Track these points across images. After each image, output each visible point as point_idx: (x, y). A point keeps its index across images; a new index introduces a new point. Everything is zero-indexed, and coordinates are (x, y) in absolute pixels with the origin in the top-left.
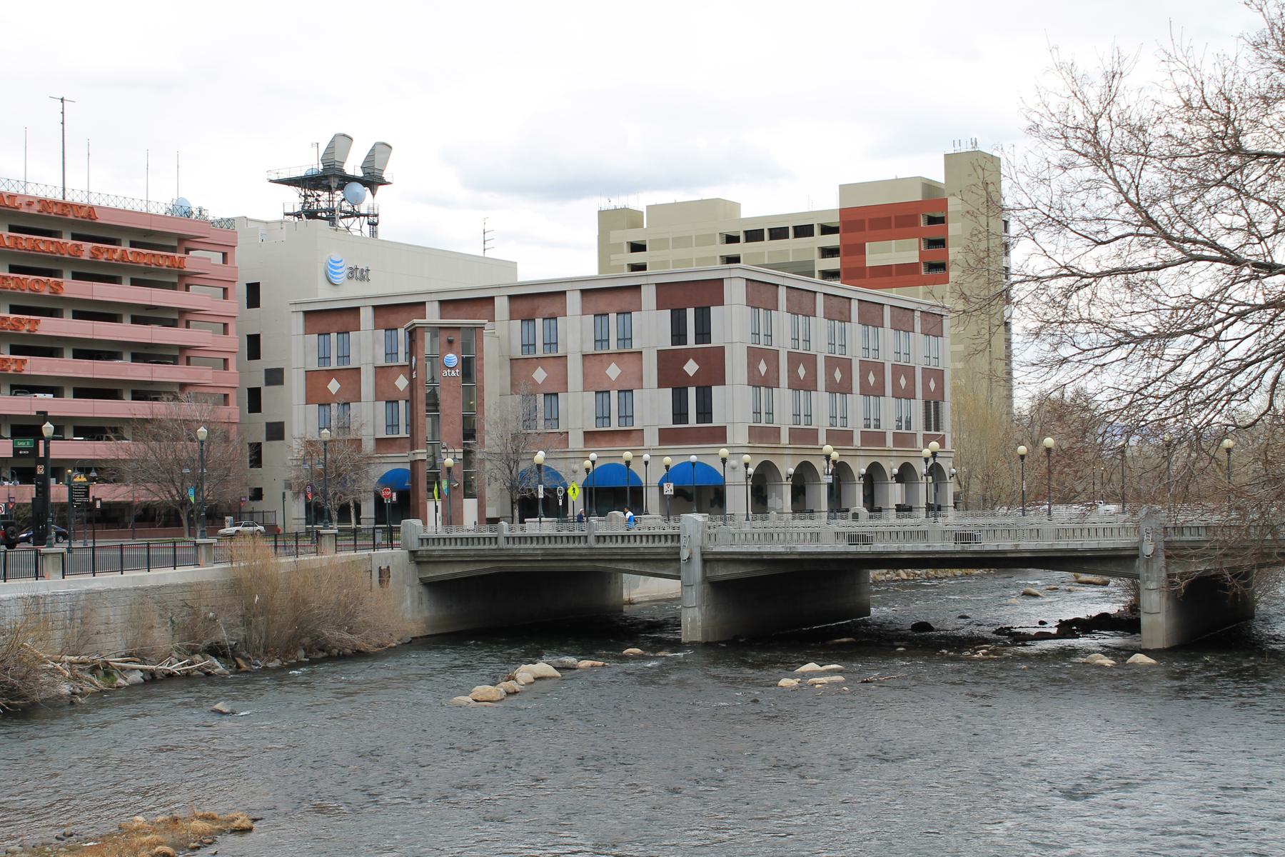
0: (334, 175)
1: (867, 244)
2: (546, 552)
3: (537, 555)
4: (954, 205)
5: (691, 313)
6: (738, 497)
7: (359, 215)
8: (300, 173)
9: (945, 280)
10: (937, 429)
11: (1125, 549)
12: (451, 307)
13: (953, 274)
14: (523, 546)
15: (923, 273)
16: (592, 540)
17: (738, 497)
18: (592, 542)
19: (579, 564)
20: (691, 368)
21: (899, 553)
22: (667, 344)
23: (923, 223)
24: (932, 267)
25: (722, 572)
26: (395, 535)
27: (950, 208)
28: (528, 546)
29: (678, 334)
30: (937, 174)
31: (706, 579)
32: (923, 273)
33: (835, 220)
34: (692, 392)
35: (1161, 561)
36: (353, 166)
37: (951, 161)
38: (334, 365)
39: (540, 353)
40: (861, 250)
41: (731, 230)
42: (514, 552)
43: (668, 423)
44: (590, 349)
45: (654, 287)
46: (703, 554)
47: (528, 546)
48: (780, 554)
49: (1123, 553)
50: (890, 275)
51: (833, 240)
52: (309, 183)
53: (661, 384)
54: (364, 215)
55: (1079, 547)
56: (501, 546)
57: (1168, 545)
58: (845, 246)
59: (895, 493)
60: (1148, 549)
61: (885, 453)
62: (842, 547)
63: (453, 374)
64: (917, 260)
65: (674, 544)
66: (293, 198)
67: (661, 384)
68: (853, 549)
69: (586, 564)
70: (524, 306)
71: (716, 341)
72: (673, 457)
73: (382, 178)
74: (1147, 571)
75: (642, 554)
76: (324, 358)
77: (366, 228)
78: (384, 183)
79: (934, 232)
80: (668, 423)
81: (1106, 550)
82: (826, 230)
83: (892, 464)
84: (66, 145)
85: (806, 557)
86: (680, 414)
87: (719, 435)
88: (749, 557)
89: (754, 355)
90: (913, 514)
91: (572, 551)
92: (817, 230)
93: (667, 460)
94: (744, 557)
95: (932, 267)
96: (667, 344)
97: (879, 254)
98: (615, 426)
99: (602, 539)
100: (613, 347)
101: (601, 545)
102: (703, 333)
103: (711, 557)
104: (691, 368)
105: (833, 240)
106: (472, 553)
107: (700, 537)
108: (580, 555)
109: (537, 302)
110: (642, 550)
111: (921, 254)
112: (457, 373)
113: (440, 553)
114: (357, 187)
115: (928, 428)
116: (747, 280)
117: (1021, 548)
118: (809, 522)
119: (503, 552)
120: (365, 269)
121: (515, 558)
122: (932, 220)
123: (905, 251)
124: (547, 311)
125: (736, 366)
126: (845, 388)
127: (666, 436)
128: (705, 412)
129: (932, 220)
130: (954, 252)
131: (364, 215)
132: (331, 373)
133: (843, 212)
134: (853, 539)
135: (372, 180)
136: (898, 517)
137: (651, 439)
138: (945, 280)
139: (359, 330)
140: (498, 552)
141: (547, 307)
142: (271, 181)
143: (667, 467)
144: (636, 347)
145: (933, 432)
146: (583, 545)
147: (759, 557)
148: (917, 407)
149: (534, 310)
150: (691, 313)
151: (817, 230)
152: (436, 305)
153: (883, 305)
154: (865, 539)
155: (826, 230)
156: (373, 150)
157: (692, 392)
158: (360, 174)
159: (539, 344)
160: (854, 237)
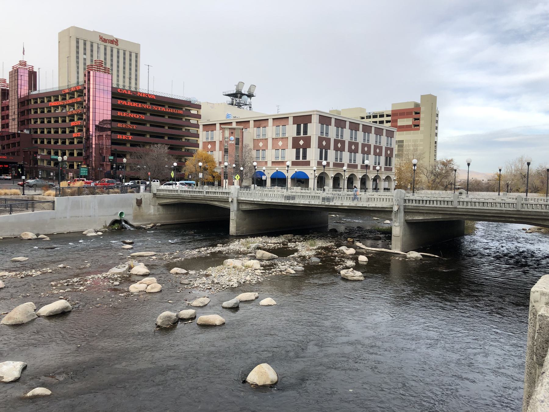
0: (239, 93)
1: (398, 120)
2: (192, 196)
3: (189, 197)
4: (422, 109)
5: (302, 125)
6: (312, 183)
7: (246, 105)
8: (230, 93)
9: (419, 129)
10: (390, 165)
11: (387, 208)
12: (239, 123)
13: (421, 128)
14: (185, 194)
15: (413, 127)
16: (204, 192)
17: (312, 183)
18: (205, 194)
19: (202, 201)
20: (301, 143)
21: (299, 204)
22: (295, 135)
23: (414, 114)
24: (415, 126)
25: (244, 207)
26: (367, 190)
27: (421, 110)
28: (187, 194)
29: (298, 133)
30: (418, 101)
31: (238, 209)
32: (413, 127)
33: (390, 113)
34: (301, 150)
35: (402, 214)
36: (245, 91)
37: (422, 97)
38: (210, 140)
39: (261, 138)
40: (396, 121)
41: (362, 116)
42: (182, 196)
43: (294, 160)
44: (274, 137)
45: (292, 117)
46: (238, 200)
47: (187, 194)
48: (259, 202)
49: (386, 209)
50: (404, 128)
51: (389, 119)
52: (234, 95)
53: (293, 148)
54: (248, 105)
55: (367, 206)
56: (179, 193)
57: (405, 208)
58: (392, 120)
59: (383, 185)
60: (395, 208)
61: (392, 173)
62: (282, 201)
63: (233, 142)
64: (411, 124)
65: (227, 196)
66: (229, 99)
67: (293, 148)
68: (287, 201)
69: (204, 201)
70: (258, 123)
71: (309, 135)
72: (297, 169)
73: (253, 95)
74: (395, 218)
75: (220, 199)
76: (207, 138)
77: (248, 108)
78: (253, 96)
79: (417, 116)
80: (294, 160)
81: (379, 208)
82: (388, 116)
83: (372, 175)
84: (284, 120)
85: (268, 203)
86: (298, 157)
87: (308, 164)
88: (251, 202)
89: (320, 140)
90: (390, 191)
91: (199, 197)
92: (385, 116)
93: (296, 170)
94: (249, 202)
95: (415, 126)
96: (295, 135)
97: (402, 122)
98: (280, 160)
99: (208, 193)
100: (281, 136)
101: (207, 195)
102: (305, 132)
103: (240, 201)
104: (301, 143)
105: (389, 119)
106: (171, 195)
107: (237, 194)
108: (201, 198)
109: (261, 122)
110: (219, 197)
111: (413, 122)
112: (233, 142)
113: (162, 195)
114: (245, 97)
115: (386, 165)
116: (320, 115)
117: (344, 205)
118: (338, 192)
119: (180, 195)
120: (12, 68)
121: (183, 198)
122: (416, 113)
123: (408, 122)
124: (263, 125)
125: (314, 142)
126: (356, 151)
127: (294, 163)
128: (305, 157)
129: (416, 113)
130: (422, 122)
131: (248, 105)
132: (209, 142)
133: (392, 111)
134: (288, 198)
135: (250, 96)
136: (361, 191)
137: (270, 164)
138: (419, 129)
139: (216, 130)
140: (178, 195)
141: (263, 124)
142: (224, 95)
143: (296, 172)
144: (287, 136)
145: (388, 166)
146: (202, 194)
147: (253, 202)
148: (383, 159)
149: (260, 125)
150: (302, 125)
151: (385, 116)
152: (235, 123)
153: (346, 121)
154: (293, 198)
155: (388, 116)
156: (250, 87)
157: (301, 150)
158: (247, 93)
159: (261, 135)
160: (395, 118)
